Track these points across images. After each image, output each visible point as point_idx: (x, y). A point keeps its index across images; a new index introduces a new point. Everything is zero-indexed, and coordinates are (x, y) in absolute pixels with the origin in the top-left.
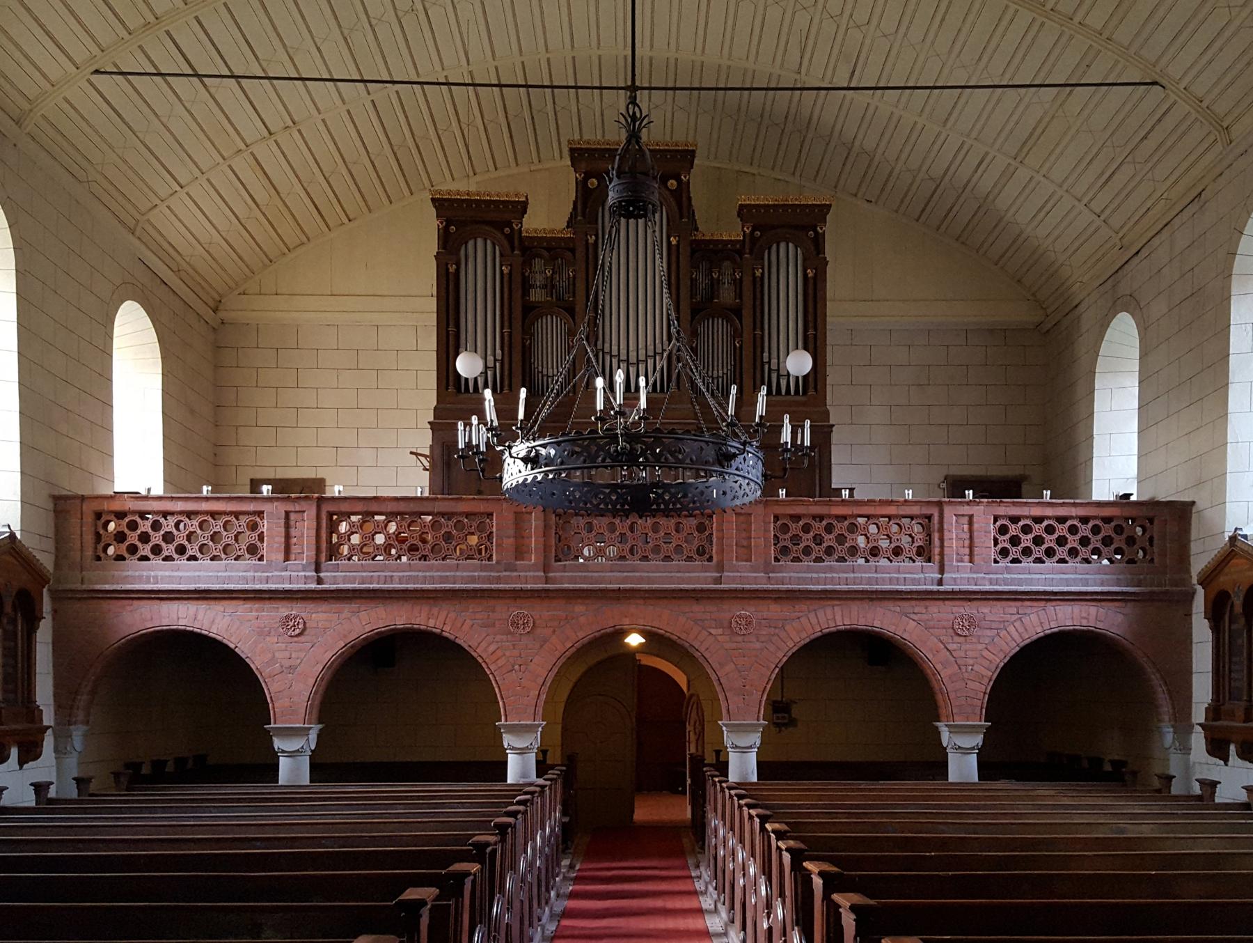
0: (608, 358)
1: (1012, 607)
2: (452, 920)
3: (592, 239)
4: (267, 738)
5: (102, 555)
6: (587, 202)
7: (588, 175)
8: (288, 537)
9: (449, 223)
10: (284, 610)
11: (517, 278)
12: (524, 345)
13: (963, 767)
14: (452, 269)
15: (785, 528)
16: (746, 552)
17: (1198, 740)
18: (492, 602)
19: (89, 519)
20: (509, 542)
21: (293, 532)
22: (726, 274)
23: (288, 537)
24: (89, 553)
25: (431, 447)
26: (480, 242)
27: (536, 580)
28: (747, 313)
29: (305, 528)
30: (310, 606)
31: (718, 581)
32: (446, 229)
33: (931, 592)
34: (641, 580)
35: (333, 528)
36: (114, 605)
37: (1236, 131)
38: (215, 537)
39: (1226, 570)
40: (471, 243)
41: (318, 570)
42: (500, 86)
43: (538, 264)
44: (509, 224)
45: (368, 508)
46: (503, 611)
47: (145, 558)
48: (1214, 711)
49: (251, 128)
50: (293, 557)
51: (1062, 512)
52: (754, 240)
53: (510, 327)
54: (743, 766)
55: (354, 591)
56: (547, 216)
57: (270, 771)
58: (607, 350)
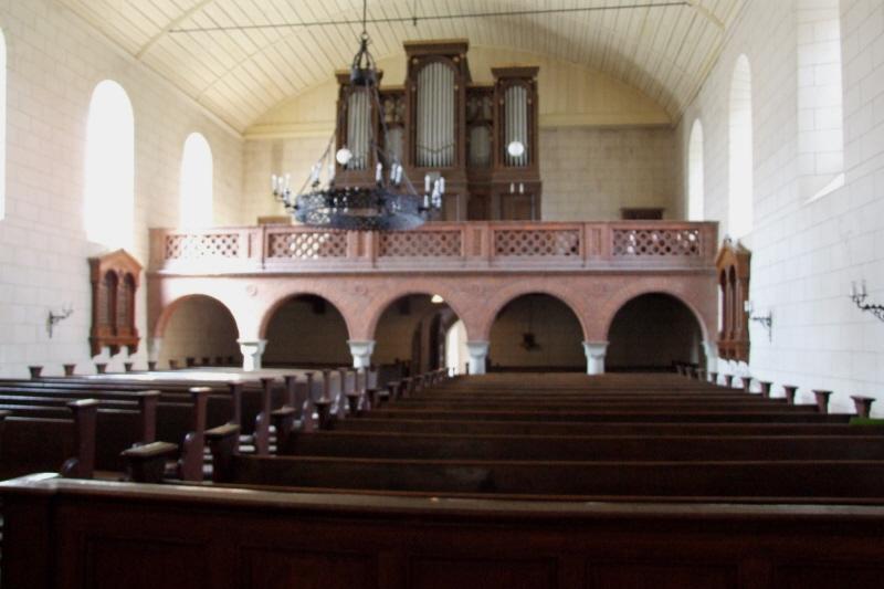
1: (621, 280)
2: (543, 497)
3: (414, 89)
6: (414, 71)
7: (413, 58)
13: (594, 366)
15: (500, 238)
16: (477, 251)
19: (164, 238)
20: (355, 247)
22: (487, 103)
28: (496, 123)
41: (263, 261)
43: (387, 103)
46: (352, 283)
49: (250, 49)
52: (498, 85)
56: (394, 75)
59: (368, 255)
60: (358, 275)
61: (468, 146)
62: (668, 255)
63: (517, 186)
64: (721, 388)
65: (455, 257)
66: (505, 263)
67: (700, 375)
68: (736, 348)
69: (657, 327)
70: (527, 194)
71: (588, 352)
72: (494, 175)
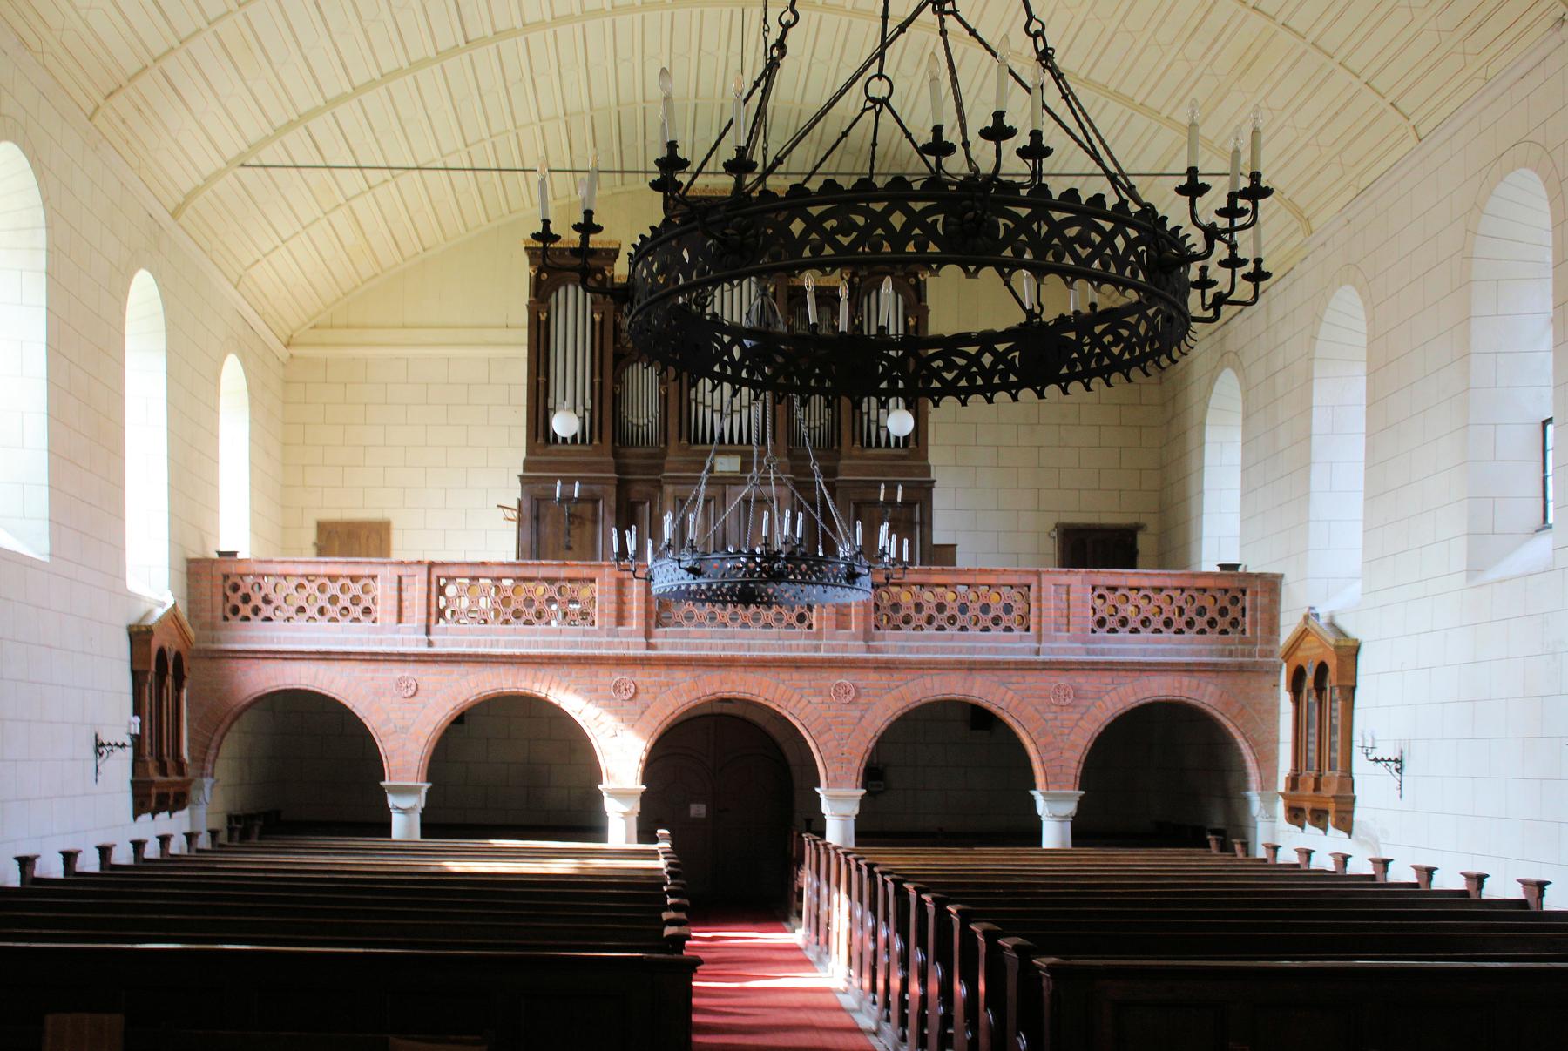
0: (708, 412)
1: (1107, 678)
4: (382, 795)
5: (230, 615)
8: (400, 600)
9: (540, 270)
10: (397, 671)
11: (609, 326)
12: (614, 395)
13: (1053, 835)
14: (543, 317)
17: (1280, 808)
18: (594, 668)
20: (611, 608)
21: (404, 595)
23: (400, 600)
24: (219, 613)
25: (520, 502)
26: (571, 288)
27: (637, 645)
29: (416, 593)
30: (421, 667)
31: (1037, 653)
32: (538, 276)
33: (1029, 663)
34: (740, 647)
35: (441, 591)
36: (243, 664)
37: (1315, 224)
38: (333, 600)
39: (1303, 646)
40: (561, 291)
41: (428, 632)
42: (622, 172)
44: (602, 271)
45: (475, 572)
47: (247, 619)
48: (1294, 782)
50: (404, 619)
51: (1157, 582)
53: (601, 375)
54: (837, 831)
55: (464, 655)
57: (385, 828)
58: (700, 399)
59: (635, 622)
60: (621, 662)
61: (617, 400)
62: (1190, 634)
63: (892, 489)
64: (1322, 874)
65: (800, 629)
66: (894, 644)
67: (1238, 847)
68: (1324, 800)
69: (1165, 768)
70: (908, 504)
71: (1042, 807)
72: (843, 462)
